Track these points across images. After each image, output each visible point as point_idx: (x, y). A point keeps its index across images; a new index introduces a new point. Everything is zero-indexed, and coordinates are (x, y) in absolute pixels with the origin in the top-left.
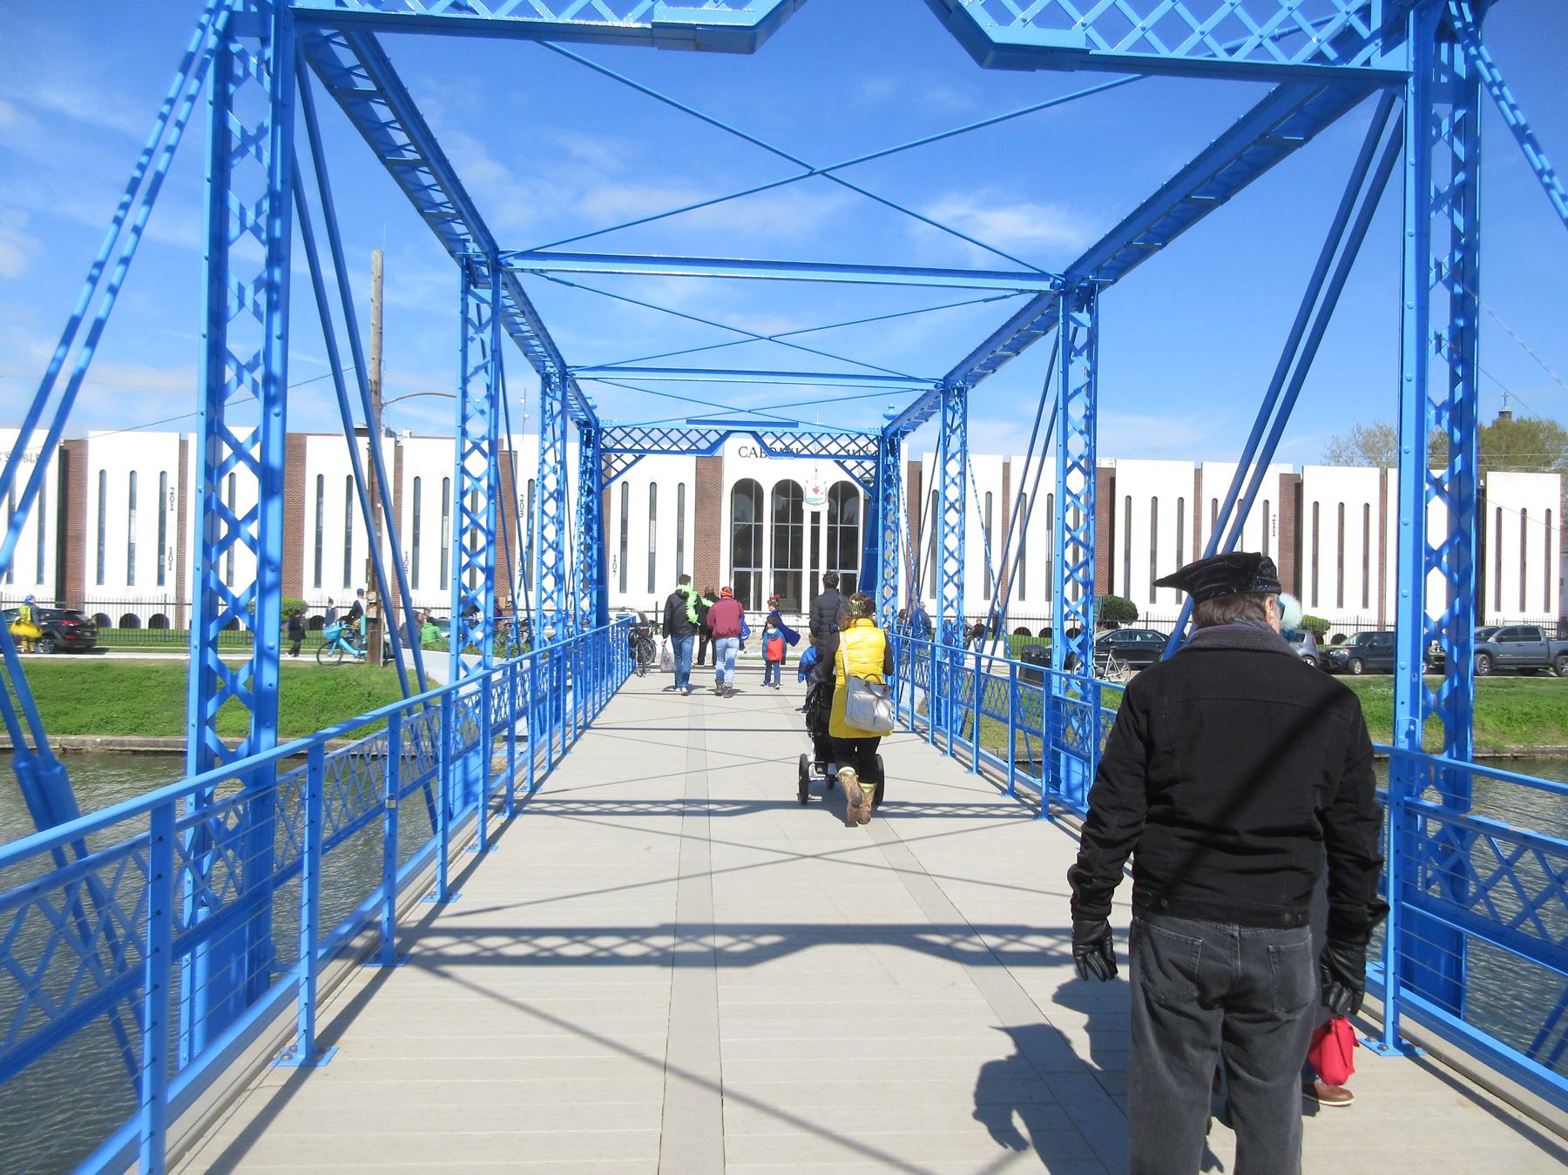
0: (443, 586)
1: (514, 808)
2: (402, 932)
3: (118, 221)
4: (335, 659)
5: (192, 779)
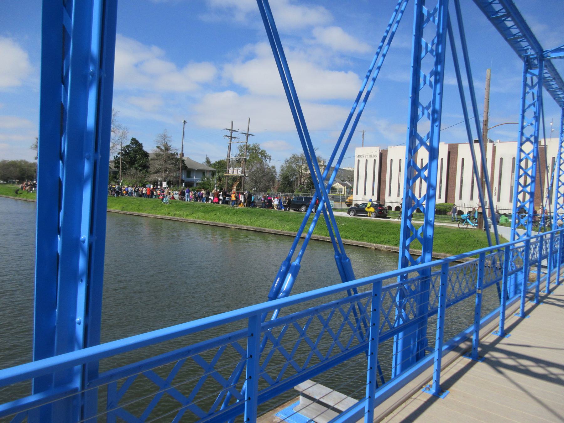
0: (511, 201)
1: (539, 300)
2: (482, 346)
3: (378, 54)
4: (465, 226)
5: (400, 270)
